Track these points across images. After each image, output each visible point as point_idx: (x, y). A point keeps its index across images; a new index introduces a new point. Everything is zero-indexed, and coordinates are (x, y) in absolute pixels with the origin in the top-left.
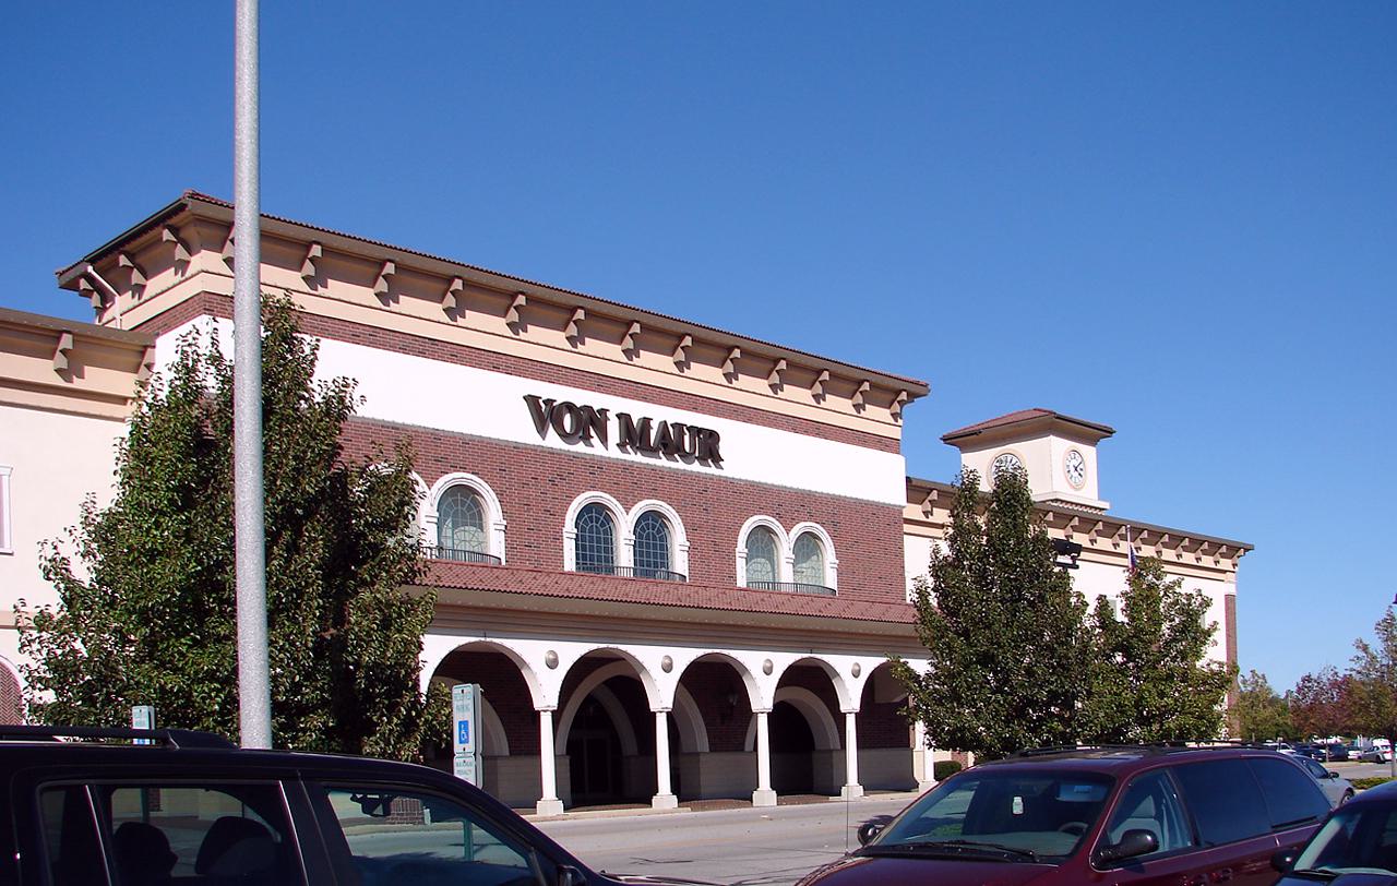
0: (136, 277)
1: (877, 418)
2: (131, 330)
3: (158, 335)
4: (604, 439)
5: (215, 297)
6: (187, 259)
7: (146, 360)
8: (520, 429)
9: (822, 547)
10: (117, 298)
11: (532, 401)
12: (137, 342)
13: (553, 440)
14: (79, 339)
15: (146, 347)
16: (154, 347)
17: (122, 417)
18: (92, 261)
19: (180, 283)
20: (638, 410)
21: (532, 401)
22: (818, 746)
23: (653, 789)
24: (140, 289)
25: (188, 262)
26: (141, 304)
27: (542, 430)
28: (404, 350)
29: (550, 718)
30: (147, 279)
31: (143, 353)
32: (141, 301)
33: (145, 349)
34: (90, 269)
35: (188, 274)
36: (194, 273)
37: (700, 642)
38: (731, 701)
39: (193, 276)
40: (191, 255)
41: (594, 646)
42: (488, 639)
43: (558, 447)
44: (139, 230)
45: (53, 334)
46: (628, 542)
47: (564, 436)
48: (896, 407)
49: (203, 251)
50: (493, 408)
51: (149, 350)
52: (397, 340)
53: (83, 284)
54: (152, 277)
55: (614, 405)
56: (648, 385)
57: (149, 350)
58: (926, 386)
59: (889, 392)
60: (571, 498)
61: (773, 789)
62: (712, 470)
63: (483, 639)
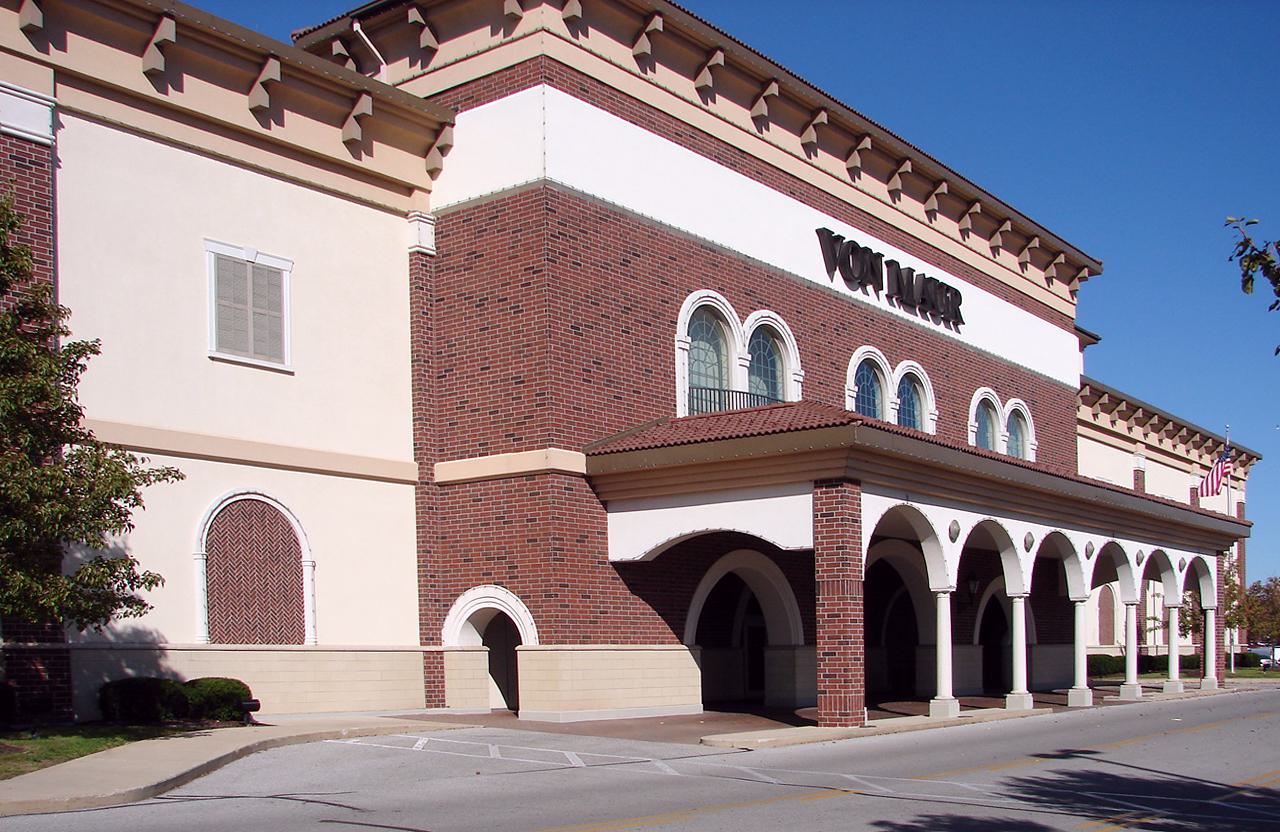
0: (427, 38)
1: (1058, 295)
2: (426, 98)
3: (456, 111)
4: (878, 288)
5: (554, 63)
6: (434, 47)
7: (440, 142)
8: (810, 266)
9: (1024, 427)
10: (384, 67)
11: (824, 235)
12: (434, 117)
13: (838, 284)
14: (381, 107)
15: (443, 125)
16: (453, 125)
17: (406, 211)
18: (361, 17)
19: (502, 45)
20: (906, 260)
21: (824, 235)
22: (922, 641)
23: (932, 692)
24: (431, 52)
25: (520, 18)
26: (425, 74)
27: (830, 272)
28: (718, 159)
29: (948, 600)
30: (439, 43)
31: (437, 133)
32: (426, 70)
33: (444, 125)
34: (357, 27)
35: (431, 67)
36: (438, 66)
37: (1052, 519)
38: (972, 588)
39: (435, 70)
40: (439, 43)
41: (987, 517)
42: (910, 503)
43: (843, 292)
44: (375, 7)
45: (343, 92)
46: (894, 406)
47: (848, 280)
48: (1076, 284)
49: (544, 4)
50: (782, 235)
51: (447, 128)
52: (713, 146)
53: (338, 48)
54: (444, 41)
55: (890, 252)
56: (916, 232)
57: (447, 128)
58: (1100, 264)
59: (1072, 268)
60: (851, 351)
61: (1030, 692)
62: (951, 333)
63: (905, 502)
